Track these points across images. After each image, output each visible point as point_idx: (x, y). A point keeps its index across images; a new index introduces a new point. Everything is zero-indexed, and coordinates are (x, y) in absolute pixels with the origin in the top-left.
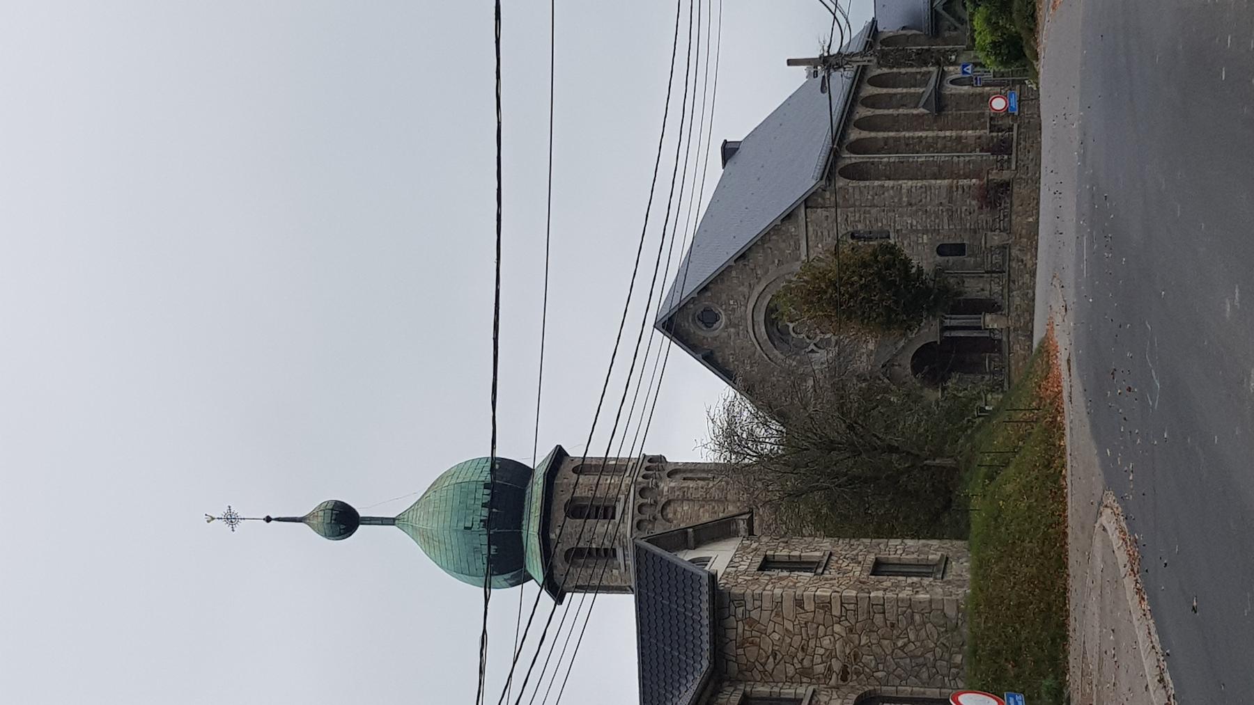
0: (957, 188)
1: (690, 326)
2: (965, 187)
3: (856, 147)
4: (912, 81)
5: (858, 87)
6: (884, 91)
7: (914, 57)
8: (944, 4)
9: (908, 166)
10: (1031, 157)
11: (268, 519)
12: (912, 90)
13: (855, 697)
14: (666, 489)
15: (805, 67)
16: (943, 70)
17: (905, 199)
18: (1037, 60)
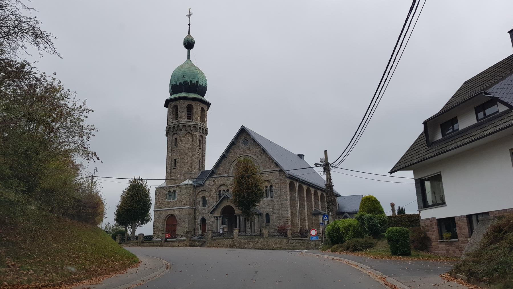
0: (287, 219)
1: (243, 137)
6: (320, 198)
10: (296, 245)
11: (189, 25)
12: (320, 206)
14: (196, 134)
15: (324, 158)
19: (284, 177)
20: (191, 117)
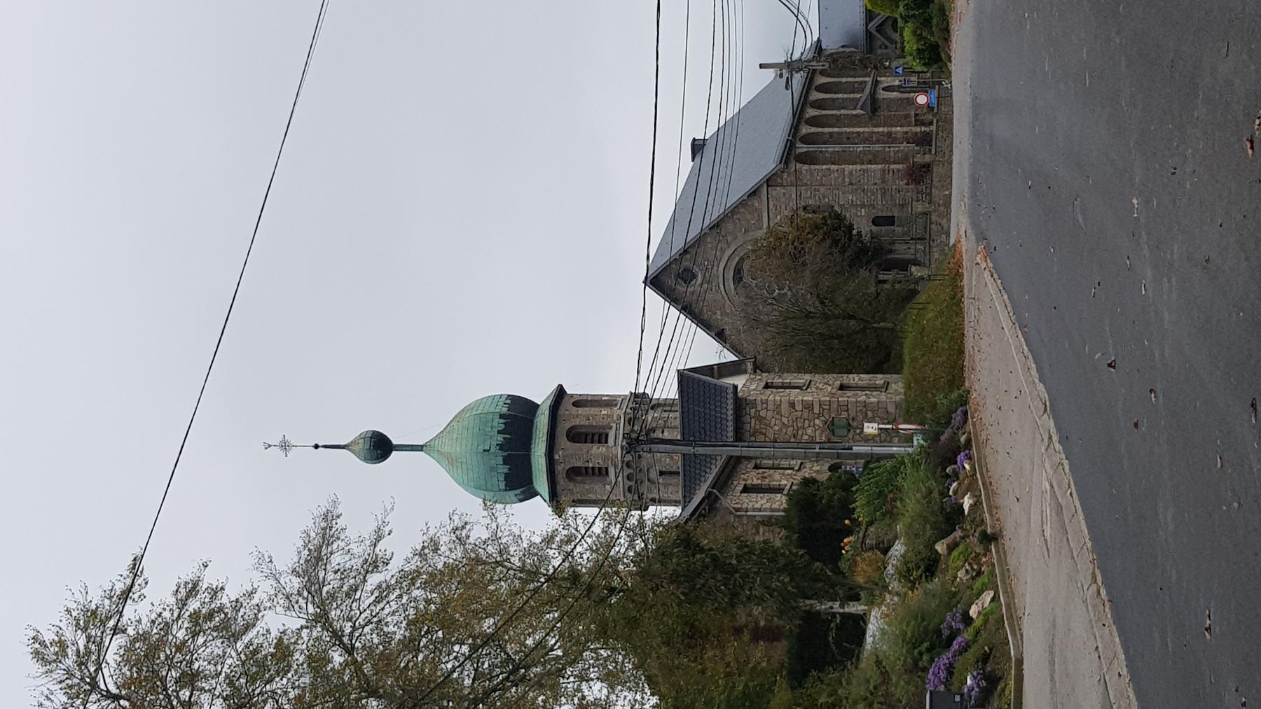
0: (889, 171)
1: (671, 282)
2: (895, 171)
3: (807, 139)
4: (852, 88)
5: (807, 92)
6: (828, 96)
7: (857, 63)
8: (876, 27)
9: (849, 155)
11: (316, 447)
12: (852, 96)
13: (829, 465)
16: (876, 79)
17: (847, 180)
18: (950, 61)
19: (785, 176)
20: (603, 433)
